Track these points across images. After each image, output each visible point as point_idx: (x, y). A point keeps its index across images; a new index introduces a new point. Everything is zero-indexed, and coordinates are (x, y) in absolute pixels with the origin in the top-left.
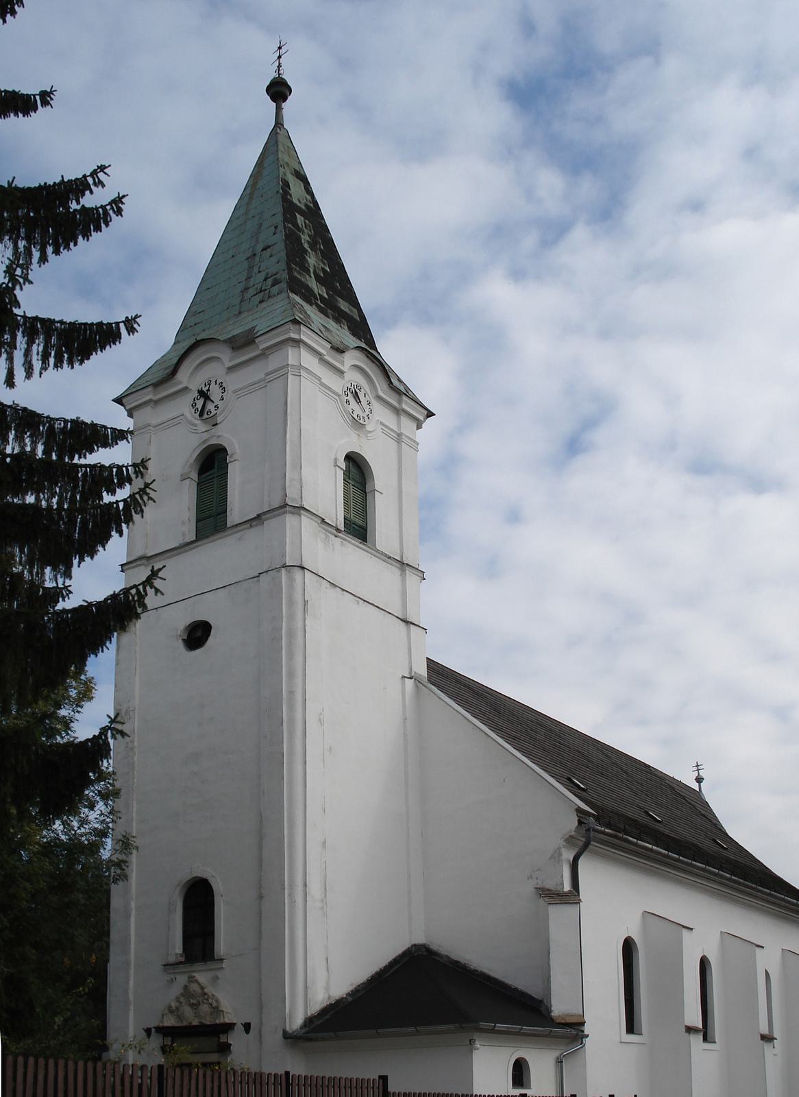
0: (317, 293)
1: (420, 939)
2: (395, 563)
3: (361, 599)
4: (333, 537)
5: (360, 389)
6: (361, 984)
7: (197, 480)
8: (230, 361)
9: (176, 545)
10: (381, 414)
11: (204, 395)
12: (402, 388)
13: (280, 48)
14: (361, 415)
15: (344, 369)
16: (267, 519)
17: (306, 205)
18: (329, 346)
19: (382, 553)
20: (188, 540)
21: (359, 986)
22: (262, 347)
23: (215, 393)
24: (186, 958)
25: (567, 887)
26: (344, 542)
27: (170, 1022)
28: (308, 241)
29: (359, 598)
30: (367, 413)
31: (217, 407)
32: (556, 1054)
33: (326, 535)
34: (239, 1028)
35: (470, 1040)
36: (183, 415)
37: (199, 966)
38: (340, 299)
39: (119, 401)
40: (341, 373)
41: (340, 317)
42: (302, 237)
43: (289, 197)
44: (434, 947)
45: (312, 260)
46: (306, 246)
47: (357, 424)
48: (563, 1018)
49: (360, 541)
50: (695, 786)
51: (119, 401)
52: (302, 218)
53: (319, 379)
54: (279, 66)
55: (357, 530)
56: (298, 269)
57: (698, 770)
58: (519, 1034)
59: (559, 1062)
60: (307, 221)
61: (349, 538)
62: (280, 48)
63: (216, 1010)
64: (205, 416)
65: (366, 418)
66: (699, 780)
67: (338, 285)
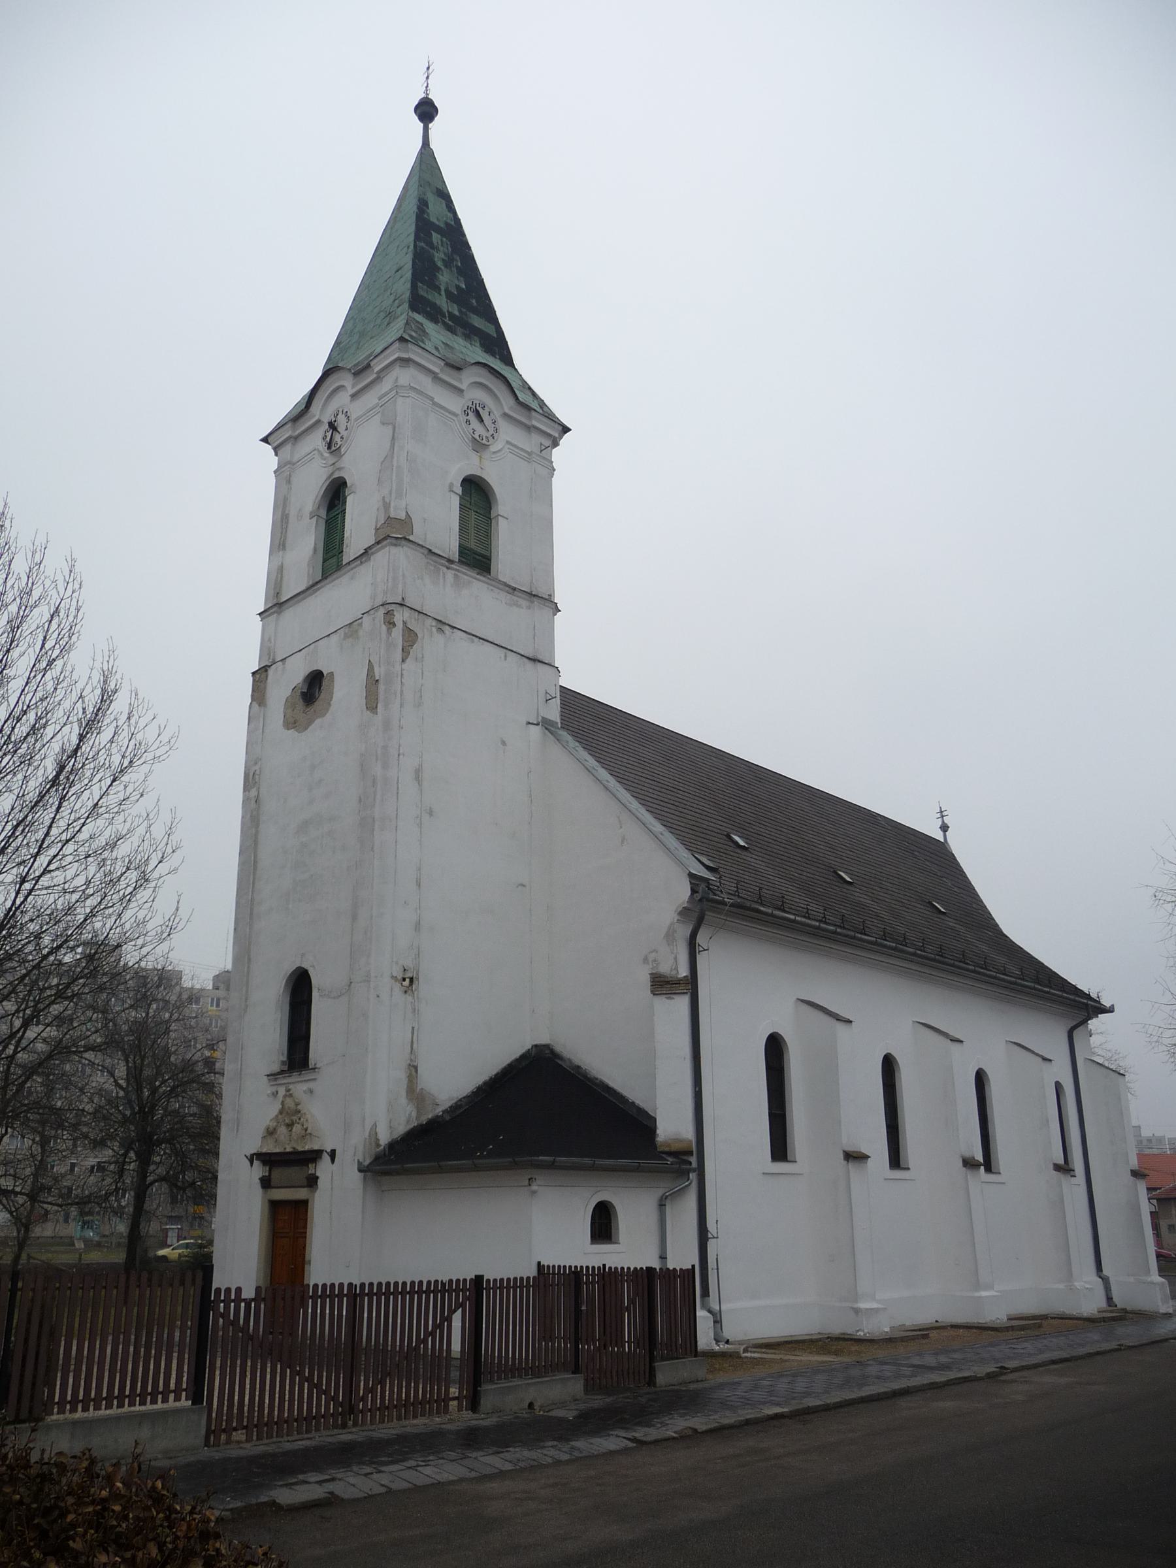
0: (445, 311)
1: (543, 1039)
2: (524, 596)
3: (477, 637)
4: (445, 569)
5: (483, 408)
6: (464, 1098)
7: (325, 517)
8: (353, 386)
9: (303, 588)
10: (508, 433)
11: (333, 426)
12: (534, 405)
13: (428, 68)
14: (484, 434)
15: (463, 386)
16: (373, 553)
17: (447, 224)
18: (442, 363)
19: (506, 585)
20: (317, 580)
21: (460, 1100)
22: (377, 369)
23: (341, 422)
24: (289, 1067)
25: (684, 972)
26: (459, 574)
27: (270, 1148)
28: (443, 260)
29: (473, 635)
30: (491, 431)
31: (342, 438)
32: (660, 1192)
33: (435, 567)
34: (326, 1158)
35: (529, 1179)
36: (315, 450)
37: (295, 1077)
38: (472, 315)
39: (265, 440)
40: (460, 391)
41: (471, 333)
42: (436, 254)
43: (425, 216)
44: (558, 1049)
45: (445, 278)
46: (440, 264)
47: (479, 446)
48: (669, 1145)
49: (478, 570)
50: (939, 836)
51: (265, 440)
52: (439, 236)
53: (432, 399)
54: (427, 87)
55: (478, 560)
56: (425, 287)
57: (942, 816)
58: (593, 1168)
59: (662, 1205)
60: (444, 239)
61: (464, 569)
62: (428, 68)
63: (306, 1134)
64: (333, 448)
65: (491, 439)
66: (944, 828)
67: (474, 301)
